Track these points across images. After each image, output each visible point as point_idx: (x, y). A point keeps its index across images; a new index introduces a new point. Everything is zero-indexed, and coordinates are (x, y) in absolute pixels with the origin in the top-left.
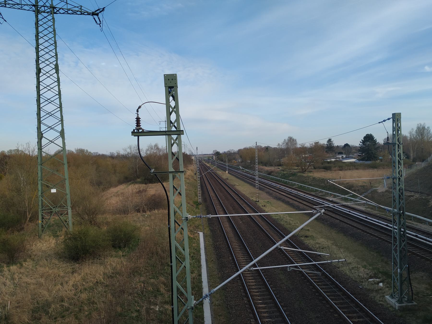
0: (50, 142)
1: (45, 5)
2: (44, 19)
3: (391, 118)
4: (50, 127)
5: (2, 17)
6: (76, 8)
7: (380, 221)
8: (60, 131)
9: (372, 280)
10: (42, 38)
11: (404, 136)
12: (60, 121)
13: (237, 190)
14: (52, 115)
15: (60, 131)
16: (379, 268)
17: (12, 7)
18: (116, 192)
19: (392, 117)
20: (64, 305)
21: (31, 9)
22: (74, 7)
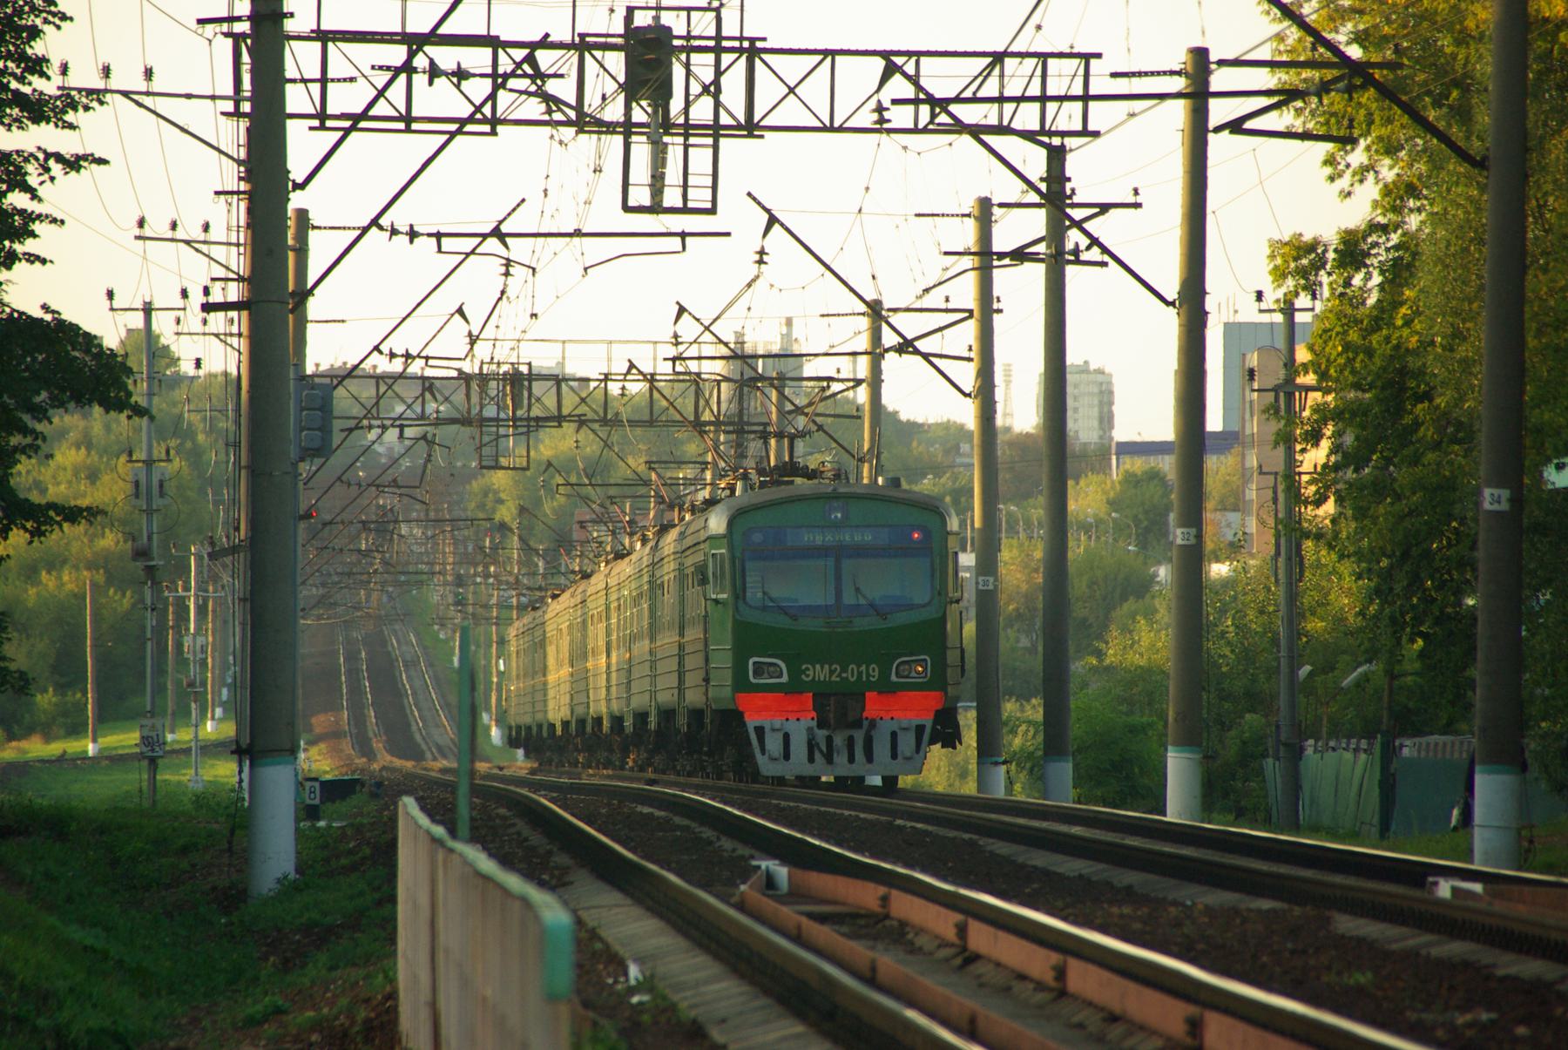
0: (974, 93)
1: (949, 121)
2: (217, 94)
3: (1218, 129)
4: (459, 131)
5: (1248, 125)
6: (919, 358)
7: (952, 834)
8: (995, 271)
9: (662, 814)
10: (909, 337)
11: (1352, 620)
12: (238, 274)
13: (928, 496)
14: (462, 126)
15: (995, 271)
16: (1325, 263)
17: (702, 403)
18: (129, 488)
19: (1043, 233)
20: (1316, 444)
21: (390, 381)
22: (935, 360)
